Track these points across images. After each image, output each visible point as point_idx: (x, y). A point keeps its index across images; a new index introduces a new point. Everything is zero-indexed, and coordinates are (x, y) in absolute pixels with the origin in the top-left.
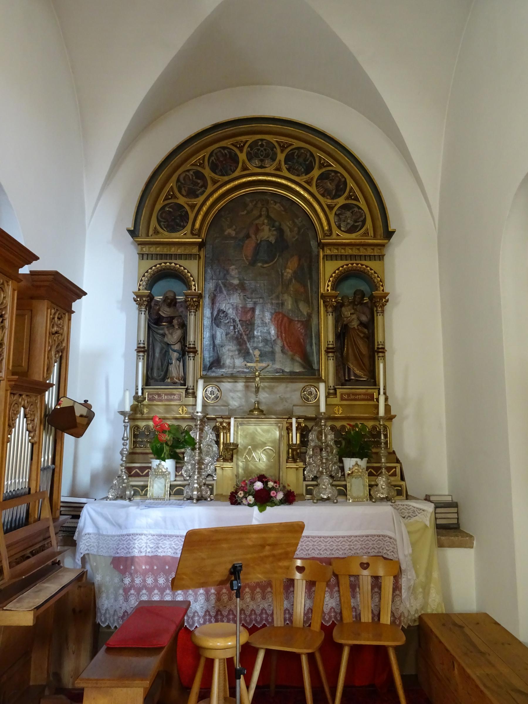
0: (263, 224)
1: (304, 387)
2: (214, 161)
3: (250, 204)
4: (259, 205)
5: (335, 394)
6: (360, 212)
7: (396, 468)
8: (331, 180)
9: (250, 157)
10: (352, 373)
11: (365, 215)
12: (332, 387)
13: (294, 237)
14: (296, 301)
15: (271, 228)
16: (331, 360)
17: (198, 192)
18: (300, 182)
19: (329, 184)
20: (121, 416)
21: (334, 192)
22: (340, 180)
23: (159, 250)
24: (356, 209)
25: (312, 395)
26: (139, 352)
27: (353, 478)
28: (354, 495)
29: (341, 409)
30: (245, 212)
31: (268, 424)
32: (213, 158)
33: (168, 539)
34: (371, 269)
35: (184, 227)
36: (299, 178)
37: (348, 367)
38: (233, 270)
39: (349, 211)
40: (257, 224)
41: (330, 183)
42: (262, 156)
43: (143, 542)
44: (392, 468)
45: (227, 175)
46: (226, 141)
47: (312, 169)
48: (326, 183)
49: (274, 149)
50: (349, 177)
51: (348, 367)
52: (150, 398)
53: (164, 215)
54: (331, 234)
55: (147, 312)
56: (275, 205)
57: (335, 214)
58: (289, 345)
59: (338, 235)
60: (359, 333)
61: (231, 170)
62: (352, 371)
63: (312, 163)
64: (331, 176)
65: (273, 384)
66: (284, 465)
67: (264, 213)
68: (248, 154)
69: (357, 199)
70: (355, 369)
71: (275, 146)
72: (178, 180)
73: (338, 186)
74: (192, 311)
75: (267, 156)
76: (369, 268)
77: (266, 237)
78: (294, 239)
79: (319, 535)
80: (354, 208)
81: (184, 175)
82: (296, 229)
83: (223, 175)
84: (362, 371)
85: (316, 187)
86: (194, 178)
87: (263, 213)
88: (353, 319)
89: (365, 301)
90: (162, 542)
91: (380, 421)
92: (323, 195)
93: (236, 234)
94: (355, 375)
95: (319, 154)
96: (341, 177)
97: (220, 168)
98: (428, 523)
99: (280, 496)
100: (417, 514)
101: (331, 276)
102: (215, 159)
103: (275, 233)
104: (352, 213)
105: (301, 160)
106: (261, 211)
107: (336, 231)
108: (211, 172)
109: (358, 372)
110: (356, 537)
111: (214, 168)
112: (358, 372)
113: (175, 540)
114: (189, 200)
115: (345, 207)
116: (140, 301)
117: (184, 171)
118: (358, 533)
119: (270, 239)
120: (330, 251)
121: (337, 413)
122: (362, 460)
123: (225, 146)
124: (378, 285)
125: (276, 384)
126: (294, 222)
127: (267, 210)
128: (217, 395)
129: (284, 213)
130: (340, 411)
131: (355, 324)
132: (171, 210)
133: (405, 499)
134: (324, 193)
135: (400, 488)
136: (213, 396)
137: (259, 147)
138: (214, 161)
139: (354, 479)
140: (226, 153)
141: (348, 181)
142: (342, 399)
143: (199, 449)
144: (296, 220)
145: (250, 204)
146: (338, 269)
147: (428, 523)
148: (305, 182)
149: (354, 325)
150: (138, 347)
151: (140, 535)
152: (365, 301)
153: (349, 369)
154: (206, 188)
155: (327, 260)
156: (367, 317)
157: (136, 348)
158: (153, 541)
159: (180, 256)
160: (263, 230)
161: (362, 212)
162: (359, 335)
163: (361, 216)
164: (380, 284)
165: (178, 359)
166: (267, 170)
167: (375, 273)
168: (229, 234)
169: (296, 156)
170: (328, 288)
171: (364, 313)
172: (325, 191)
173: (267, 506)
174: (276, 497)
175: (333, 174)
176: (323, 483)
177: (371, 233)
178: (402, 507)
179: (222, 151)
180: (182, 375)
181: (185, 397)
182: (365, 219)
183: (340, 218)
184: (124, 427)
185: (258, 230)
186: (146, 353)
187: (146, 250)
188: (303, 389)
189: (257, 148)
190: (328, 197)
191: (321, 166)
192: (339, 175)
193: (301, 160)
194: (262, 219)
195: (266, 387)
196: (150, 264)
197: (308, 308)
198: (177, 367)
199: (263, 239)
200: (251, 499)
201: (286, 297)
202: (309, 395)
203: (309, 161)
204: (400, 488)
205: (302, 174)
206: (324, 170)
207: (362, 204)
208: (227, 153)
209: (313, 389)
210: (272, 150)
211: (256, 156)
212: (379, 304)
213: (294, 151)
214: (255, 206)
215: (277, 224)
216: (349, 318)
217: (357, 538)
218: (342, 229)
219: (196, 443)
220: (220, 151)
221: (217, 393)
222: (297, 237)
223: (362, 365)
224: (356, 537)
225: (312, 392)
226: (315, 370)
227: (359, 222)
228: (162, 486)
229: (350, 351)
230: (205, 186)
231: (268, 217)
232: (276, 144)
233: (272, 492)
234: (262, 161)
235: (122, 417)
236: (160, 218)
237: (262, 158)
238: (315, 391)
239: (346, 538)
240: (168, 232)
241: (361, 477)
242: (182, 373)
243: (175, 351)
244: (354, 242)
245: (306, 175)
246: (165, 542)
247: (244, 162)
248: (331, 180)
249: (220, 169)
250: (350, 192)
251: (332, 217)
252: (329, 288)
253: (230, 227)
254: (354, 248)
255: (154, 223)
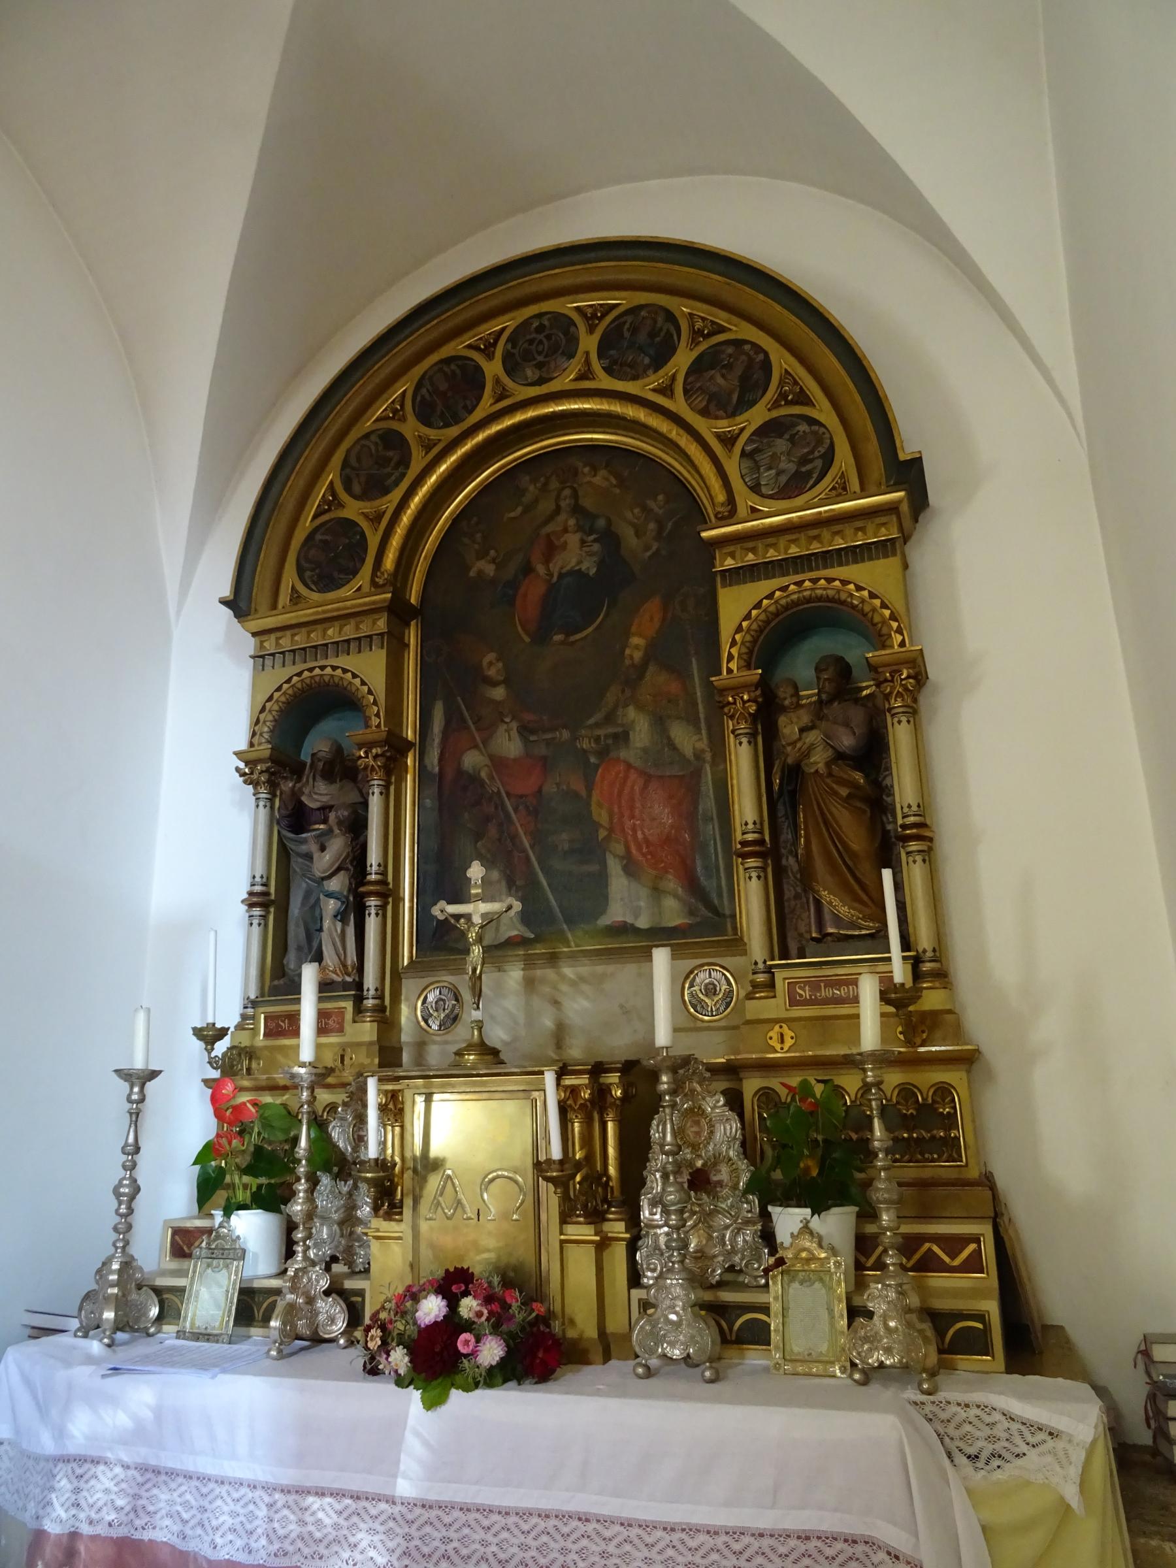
0: (566, 530)
1: (691, 972)
2: (427, 396)
3: (531, 488)
4: (554, 484)
5: (771, 985)
6: (815, 433)
7: (978, 1241)
8: (724, 366)
9: (512, 366)
10: (827, 917)
11: (831, 438)
12: (761, 966)
13: (647, 548)
14: (660, 723)
15: (585, 538)
16: (754, 879)
17: (389, 482)
18: (640, 394)
19: (720, 380)
20: (122, 1082)
21: (735, 397)
22: (751, 360)
23: (301, 640)
24: (803, 427)
25: (715, 994)
26: (251, 906)
27: (792, 1280)
28: (796, 1349)
29: (788, 1034)
30: (520, 509)
31: (485, 1096)
32: (424, 391)
33: (165, 1483)
34: (859, 588)
35: (355, 572)
36: (640, 382)
37: (814, 897)
38: (491, 664)
39: (780, 436)
40: (548, 535)
41: (723, 376)
42: (540, 353)
43: (99, 1486)
44: (965, 1240)
45: (457, 423)
46: (453, 344)
47: (673, 350)
48: (712, 378)
49: (572, 329)
50: (776, 345)
51: (814, 897)
52: (271, 1030)
53: (313, 552)
54: (733, 512)
55: (770, 870)
56: (595, 475)
57: (743, 454)
58: (644, 850)
59: (754, 510)
60: (835, 786)
61: (465, 407)
62: (826, 911)
63: (672, 336)
64: (723, 356)
65: (600, 969)
66: (552, 1235)
67: (568, 501)
68: (507, 359)
69: (803, 399)
70: (836, 902)
71: (570, 319)
72: (345, 464)
73: (744, 379)
74: (376, 782)
75: (554, 350)
76: (852, 586)
77: (573, 562)
78: (648, 554)
79: (624, 1515)
80: (794, 425)
81: (358, 447)
82: (652, 526)
83: (447, 425)
84: (856, 905)
85: (685, 395)
86: (380, 448)
87: (563, 504)
88: (811, 748)
89: (865, 693)
90: (147, 1491)
91: (864, 1071)
92: (705, 413)
93: (497, 569)
94: (838, 920)
95: (683, 308)
96: (752, 353)
97: (440, 407)
98: (1071, 1494)
99: (491, 1351)
100: (1023, 1448)
101: (739, 629)
102: (428, 390)
103: (596, 547)
104: (792, 440)
105: (642, 337)
106: (558, 498)
107: (745, 499)
108: (420, 424)
109: (844, 911)
110: (761, 1535)
111: (426, 415)
112: (844, 911)
113: (183, 1488)
114: (368, 504)
115: (769, 429)
116: (252, 773)
117: (359, 440)
118: (765, 1520)
119: (584, 567)
120: (733, 558)
121: (778, 1046)
122: (455, 1268)
123: (453, 353)
124: (885, 630)
125: (610, 968)
126: (645, 509)
127: (575, 495)
128: (452, 1011)
129: (618, 491)
130: (789, 1042)
131: (819, 759)
132: (328, 538)
133: (1003, 1368)
134: (707, 406)
135: (980, 1326)
136: (443, 1016)
137: (534, 335)
138: (427, 396)
139: (796, 1285)
140: (453, 372)
141: (773, 358)
142: (794, 1002)
143: (307, 1180)
144: (651, 504)
145: (531, 488)
146: (758, 605)
147: (1071, 1494)
148: (654, 390)
149: (816, 763)
150: (251, 894)
151: (93, 1461)
152: (865, 693)
153: (818, 904)
154: (407, 467)
155: (724, 586)
156: (854, 734)
157: (245, 896)
158: (124, 1485)
159: (343, 647)
160: (564, 546)
161: (822, 430)
162: (835, 793)
163: (820, 442)
164: (891, 627)
165: (341, 916)
166: (554, 386)
167: (872, 595)
168: (480, 573)
169: (628, 330)
170: (731, 665)
171: (847, 724)
172: (709, 402)
173: (453, 1385)
174: (474, 1353)
175: (730, 350)
176: (668, 1302)
177: (854, 484)
178: (962, 1414)
179: (446, 369)
180: (353, 961)
181: (354, 1021)
182: (832, 447)
183: (755, 460)
184: (128, 1115)
185: (551, 549)
186: (272, 910)
187: (270, 645)
188: (687, 977)
189: (528, 337)
190: (721, 413)
191: (697, 335)
192: (747, 347)
193: (642, 337)
194: (562, 518)
195: (582, 979)
196: (279, 674)
197: (695, 738)
198: (337, 940)
199: (564, 571)
200: (399, 1358)
201: (632, 713)
202: (707, 995)
203: (662, 334)
204: (980, 1326)
205: (645, 371)
206: (703, 347)
207: (824, 412)
208: (458, 371)
209: (719, 975)
210: (566, 333)
211: (527, 356)
212: (893, 688)
213: (622, 320)
214: (544, 488)
215: (601, 523)
216: (799, 745)
217: (766, 1542)
218: (764, 490)
219: (299, 1161)
220: (441, 370)
221: (454, 1006)
222: (655, 547)
223: (856, 887)
224: (761, 1535)
225: (715, 986)
226: (724, 915)
227: (811, 461)
228: (219, 1293)
229: (815, 848)
230: (405, 462)
231: (577, 510)
232: (576, 317)
233: (465, 1336)
234: (540, 366)
235: (125, 1086)
236: (303, 562)
237: (540, 358)
238: (723, 981)
239: (724, 1538)
240: (319, 592)
241: (821, 1280)
242: (352, 957)
243: (330, 895)
244: (800, 517)
245: (656, 371)
246: (155, 1491)
247: (497, 381)
248: (724, 366)
249: (439, 413)
250: (781, 383)
251: (732, 466)
252: (733, 665)
253: (481, 555)
254: (802, 536)
255: (290, 577)
